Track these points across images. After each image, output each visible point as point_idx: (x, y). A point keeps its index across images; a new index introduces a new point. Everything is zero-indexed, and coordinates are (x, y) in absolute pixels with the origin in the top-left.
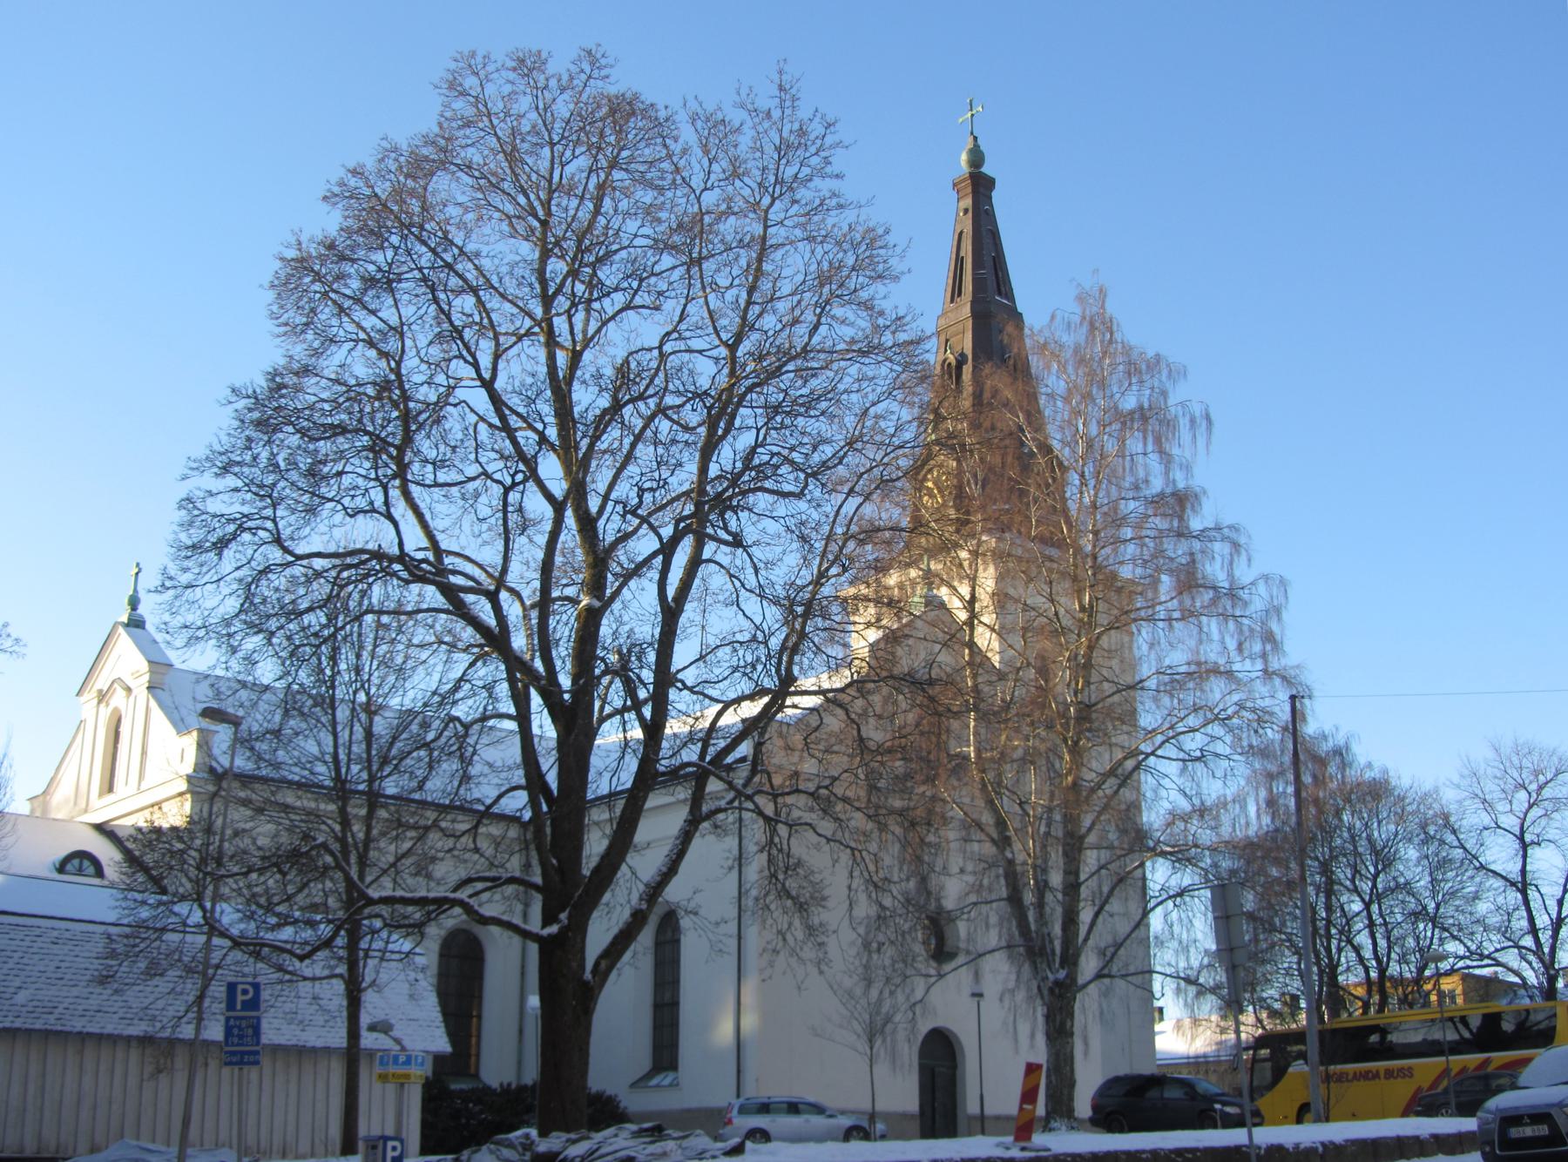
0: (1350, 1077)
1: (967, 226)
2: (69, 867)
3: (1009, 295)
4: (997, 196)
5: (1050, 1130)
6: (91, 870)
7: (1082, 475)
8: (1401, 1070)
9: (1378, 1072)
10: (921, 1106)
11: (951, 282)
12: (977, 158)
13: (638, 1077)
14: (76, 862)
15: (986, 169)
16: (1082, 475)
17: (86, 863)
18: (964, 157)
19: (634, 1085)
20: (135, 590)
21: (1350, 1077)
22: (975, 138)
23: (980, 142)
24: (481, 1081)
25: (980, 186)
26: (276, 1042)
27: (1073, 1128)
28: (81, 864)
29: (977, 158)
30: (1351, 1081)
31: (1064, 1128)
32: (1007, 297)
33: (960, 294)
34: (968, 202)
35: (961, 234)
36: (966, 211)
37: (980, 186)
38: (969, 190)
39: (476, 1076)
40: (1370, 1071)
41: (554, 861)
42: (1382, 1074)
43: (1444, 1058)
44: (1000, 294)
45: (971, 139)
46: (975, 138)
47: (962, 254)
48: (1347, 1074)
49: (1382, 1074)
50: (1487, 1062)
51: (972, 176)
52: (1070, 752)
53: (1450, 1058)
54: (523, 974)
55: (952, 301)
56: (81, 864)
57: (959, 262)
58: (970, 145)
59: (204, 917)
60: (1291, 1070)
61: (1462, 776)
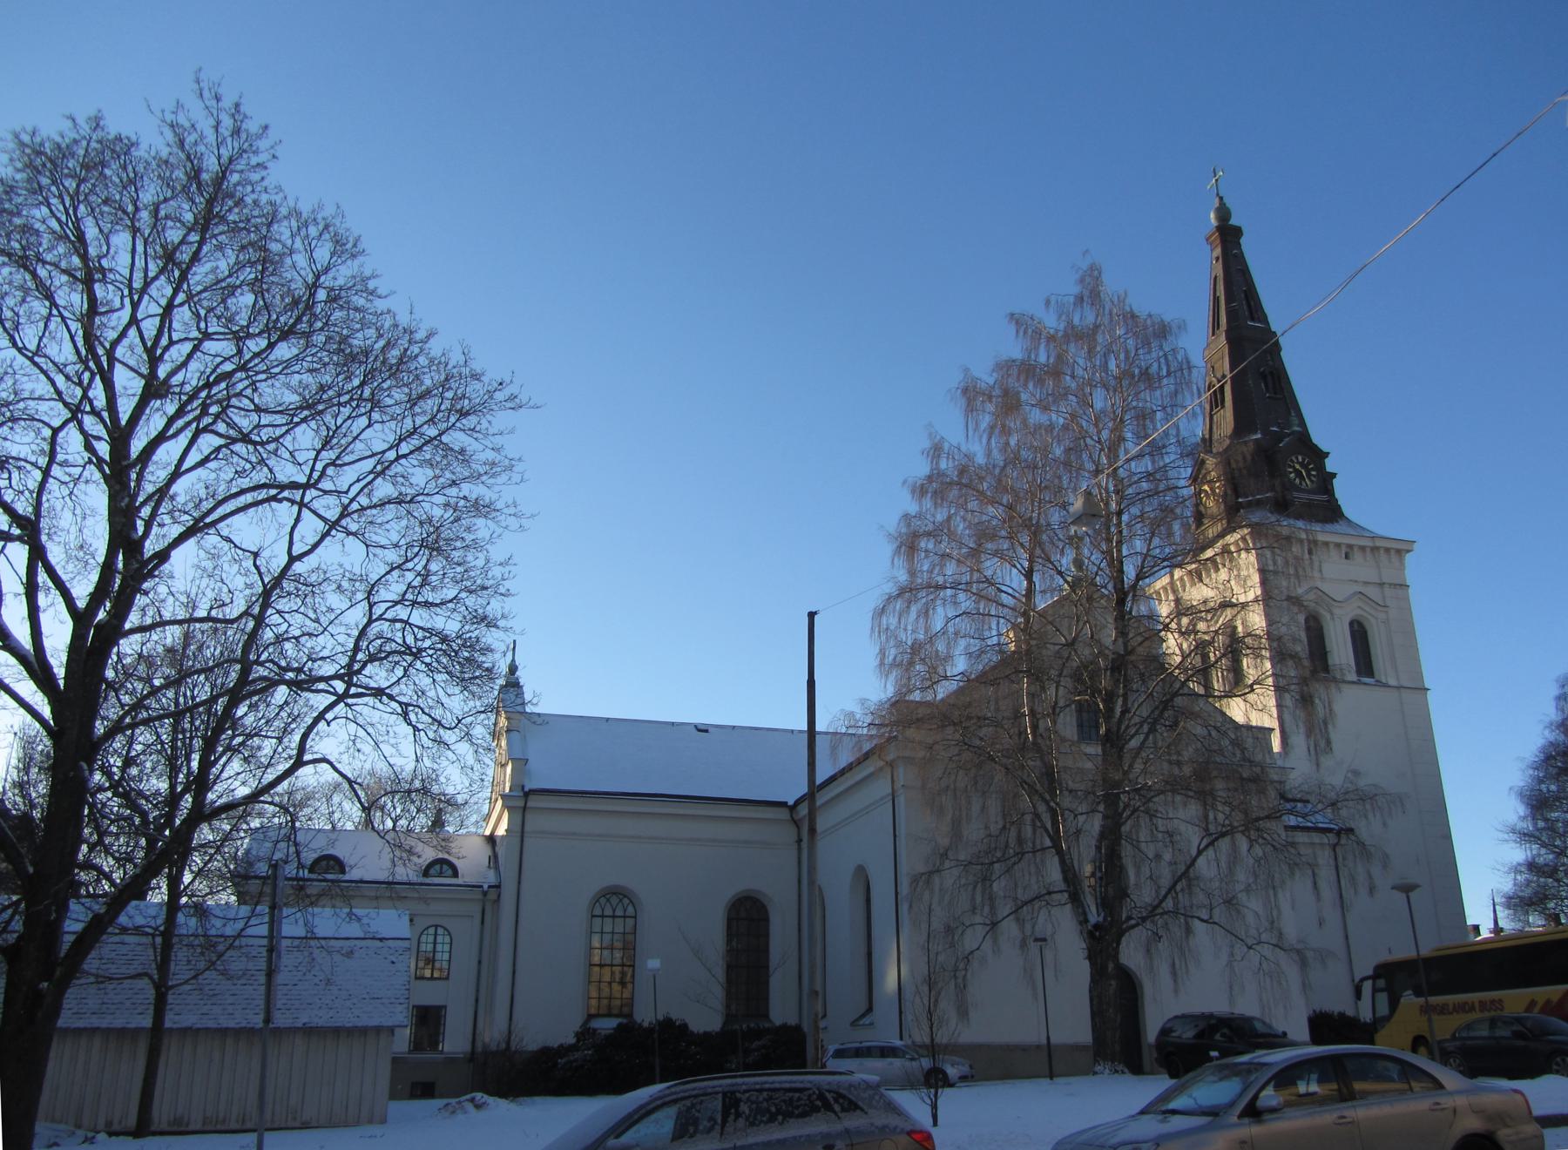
1: (1219, 270)
2: (432, 871)
3: (1264, 319)
5: (1095, 1073)
6: (450, 872)
8: (1493, 1002)
9: (1473, 1003)
10: (1094, 1039)
11: (1211, 319)
12: (1223, 213)
14: (437, 867)
15: (1233, 221)
17: (445, 867)
18: (1212, 215)
22: (1221, 198)
23: (1225, 200)
24: (770, 1021)
25: (1228, 235)
26: (225, 1026)
27: (1117, 1071)
28: (441, 868)
29: (1223, 213)
30: (1451, 1013)
32: (1260, 322)
33: (1218, 328)
34: (1218, 252)
35: (1216, 277)
36: (1217, 259)
37: (1228, 235)
38: (1218, 241)
39: (766, 1016)
40: (1466, 1003)
41: (31, 870)
42: (1477, 1005)
43: (1423, 999)
44: (1253, 319)
45: (1217, 200)
46: (1221, 198)
47: (1218, 294)
48: (1447, 1005)
49: (1477, 1005)
52: (1103, 700)
53: (1429, 998)
54: (799, 930)
55: (1213, 335)
56: (441, 868)
57: (1216, 300)
58: (1216, 203)
60: (1402, 1000)
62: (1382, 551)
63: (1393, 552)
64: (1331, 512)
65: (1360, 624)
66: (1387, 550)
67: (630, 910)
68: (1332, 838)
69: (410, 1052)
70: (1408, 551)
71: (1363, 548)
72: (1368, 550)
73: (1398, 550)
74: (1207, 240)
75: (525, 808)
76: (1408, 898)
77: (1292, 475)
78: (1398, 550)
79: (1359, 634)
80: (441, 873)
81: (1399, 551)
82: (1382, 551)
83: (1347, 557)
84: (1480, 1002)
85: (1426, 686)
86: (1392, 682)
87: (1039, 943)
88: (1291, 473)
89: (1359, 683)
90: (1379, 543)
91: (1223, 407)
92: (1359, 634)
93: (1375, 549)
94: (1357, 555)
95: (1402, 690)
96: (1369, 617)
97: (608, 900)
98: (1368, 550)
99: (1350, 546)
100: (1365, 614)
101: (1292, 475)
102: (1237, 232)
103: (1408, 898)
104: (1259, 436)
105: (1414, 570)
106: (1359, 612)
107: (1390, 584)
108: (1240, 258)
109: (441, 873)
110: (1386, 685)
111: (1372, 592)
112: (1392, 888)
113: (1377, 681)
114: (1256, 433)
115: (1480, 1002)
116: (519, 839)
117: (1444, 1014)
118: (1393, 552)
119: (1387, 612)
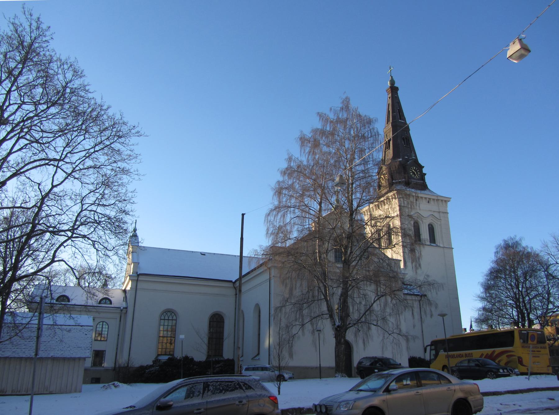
0: (455, 356)
2: (102, 302)
3: (404, 119)
4: (400, 93)
5: (335, 377)
6: (109, 302)
7: (81, 88)
11: (387, 116)
12: (392, 82)
13: (255, 355)
14: (104, 301)
15: (396, 85)
16: (81, 88)
17: (107, 301)
18: (389, 83)
19: (252, 359)
20: (135, 227)
21: (455, 356)
22: (392, 77)
25: (394, 90)
27: (343, 376)
28: (106, 301)
29: (392, 82)
30: (455, 358)
31: (340, 376)
32: (403, 120)
34: (390, 95)
36: (390, 98)
37: (394, 90)
38: (390, 91)
39: (222, 356)
40: (460, 354)
42: (464, 355)
44: (401, 119)
45: (391, 77)
46: (392, 77)
48: (454, 355)
49: (464, 355)
50: (494, 352)
51: (391, 87)
55: (387, 124)
56: (106, 301)
57: (389, 112)
58: (390, 78)
59: (549, 304)
61: (542, 248)
62: (440, 201)
63: (444, 201)
64: (424, 187)
65: (432, 225)
66: (442, 200)
67: (175, 318)
68: (419, 298)
69: (91, 367)
70: (449, 201)
71: (434, 200)
72: (435, 200)
73: (445, 201)
74: (387, 91)
75: (137, 280)
76: (443, 318)
77: (412, 173)
78: (445, 201)
79: (431, 229)
80: (105, 302)
81: (445, 201)
82: (440, 201)
83: (428, 202)
84: (465, 354)
85: (453, 247)
86: (441, 245)
87: (318, 332)
88: (411, 173)
89: (430, 245)
90: (439, 198)
91: (389, 149)
92: (431, 229)
93: (437, 200)
94: (432, 202)
95: (445, 248)
96: (435, 224)
97: (167, 314)
98: (435, 200)
99: (430, 199)
100: (434, 222)
101: (412, 173)
102: (397, 89)
103: (443, 318)
104: (401, 159)
105: (450, 207)
106: (432, 221)
107: (442, 212)
108: (397, 98)
109: (105, 302)
110: (439, 247)
111: (436, 215)
112: (438, 315)
113: (436, 245)
114: (400, 158)
115: (465, 354)
116: (135, 291)
117: (453, 358)
118: (444, 201)
119: (441, 222)
